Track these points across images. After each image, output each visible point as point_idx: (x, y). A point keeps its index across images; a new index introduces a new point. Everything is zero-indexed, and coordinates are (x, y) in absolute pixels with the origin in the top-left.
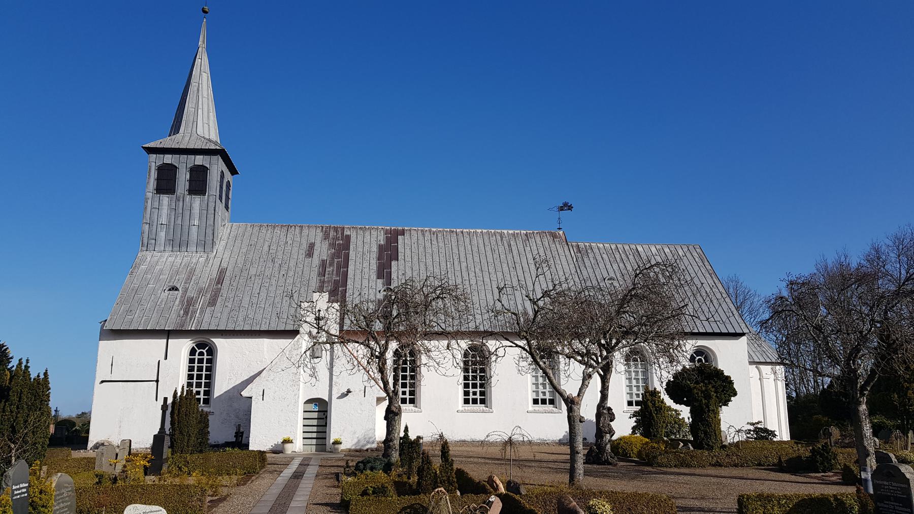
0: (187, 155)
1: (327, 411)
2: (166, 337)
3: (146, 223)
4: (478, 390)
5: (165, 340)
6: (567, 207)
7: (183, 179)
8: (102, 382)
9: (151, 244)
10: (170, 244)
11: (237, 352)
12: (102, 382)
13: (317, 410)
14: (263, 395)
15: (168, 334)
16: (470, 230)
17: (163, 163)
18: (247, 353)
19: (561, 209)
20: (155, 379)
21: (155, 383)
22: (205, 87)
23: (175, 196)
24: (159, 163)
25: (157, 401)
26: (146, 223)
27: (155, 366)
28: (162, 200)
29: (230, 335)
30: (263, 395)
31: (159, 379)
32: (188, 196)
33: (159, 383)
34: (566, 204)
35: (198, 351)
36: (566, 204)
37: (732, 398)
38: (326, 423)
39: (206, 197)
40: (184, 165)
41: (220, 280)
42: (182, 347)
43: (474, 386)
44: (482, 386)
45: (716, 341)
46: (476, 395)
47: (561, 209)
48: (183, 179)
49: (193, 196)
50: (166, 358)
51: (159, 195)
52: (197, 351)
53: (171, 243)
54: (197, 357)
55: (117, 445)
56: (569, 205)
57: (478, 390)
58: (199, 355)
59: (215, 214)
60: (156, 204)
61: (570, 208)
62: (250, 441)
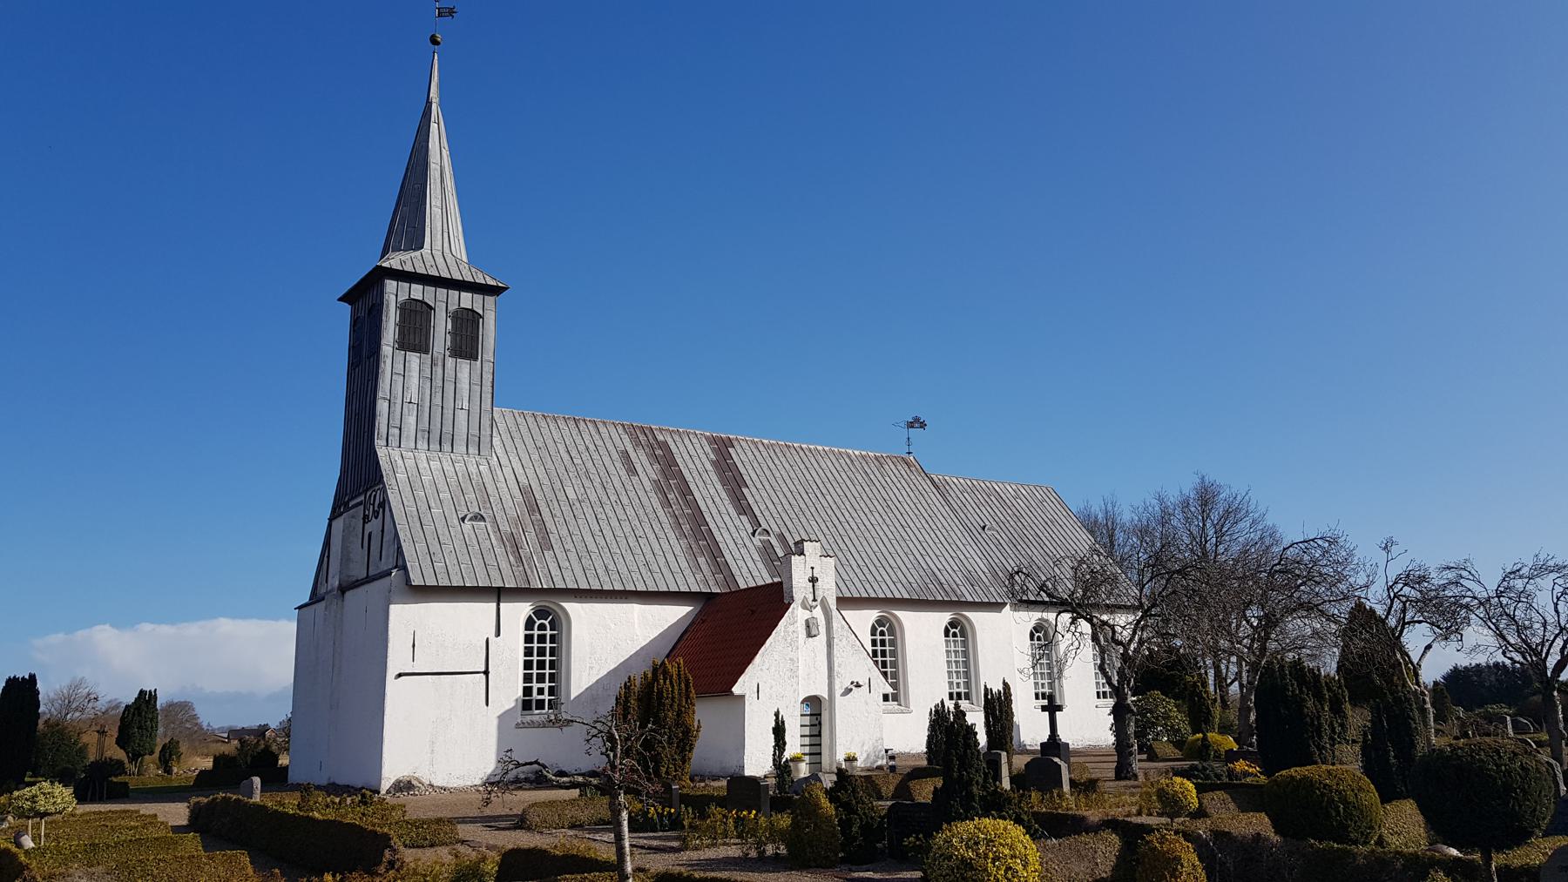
0: (448, 288)
1: (820, 715)
2: (496, 599)
3: (385, 399)
4: (546, 685)
5: (495, 604)
6: (917, 423)
7: (441, 328)
8: (400, 675)
9: (393, 435)
10: (423, 438)
11: (598, 625)
12: (400, 675)
13: (809, 713)
14: (758, 692)
15: (499, 594)
16: (840, 450)
17: (410, 299)
18: (613, 626)
19: (911, 425)
20: (483, 670)
21: (483, 676)
22: (447, 173)
23: (430, 356)
24: (403, 297)
25: (487, 705)
26: (385, 399)
27: (481, 648)
28: (410, 361)
29: (621, 598)
30: (758, 692)
31: (490, 670)
32: (450, 359)
33: (490, 675)
34: (917, 420)
35: (538, 622)
36: (917, 420)
37: (199, 721)
38: (820, 732)
39: (479, 362)
40: (444, 304)
41: (533, 507)
42: (517, 613)
43: (541, 678)
44: (552, 678)
45: (515, 604)
46: (543, 694)
47: (911, 425)
48: (441, 328)
49: (458, 360)
50: (498, 634)
51: (403, 352)
52: (535, 622)
53: (426, 436)
54: (536, 632)
55: (428, 783)
56: (921, 421)
57: (546, 685)
58: (538, 630)
59: (493, 394)
60: (399, 367)
61: (923, 425)
62: (745, 761)
